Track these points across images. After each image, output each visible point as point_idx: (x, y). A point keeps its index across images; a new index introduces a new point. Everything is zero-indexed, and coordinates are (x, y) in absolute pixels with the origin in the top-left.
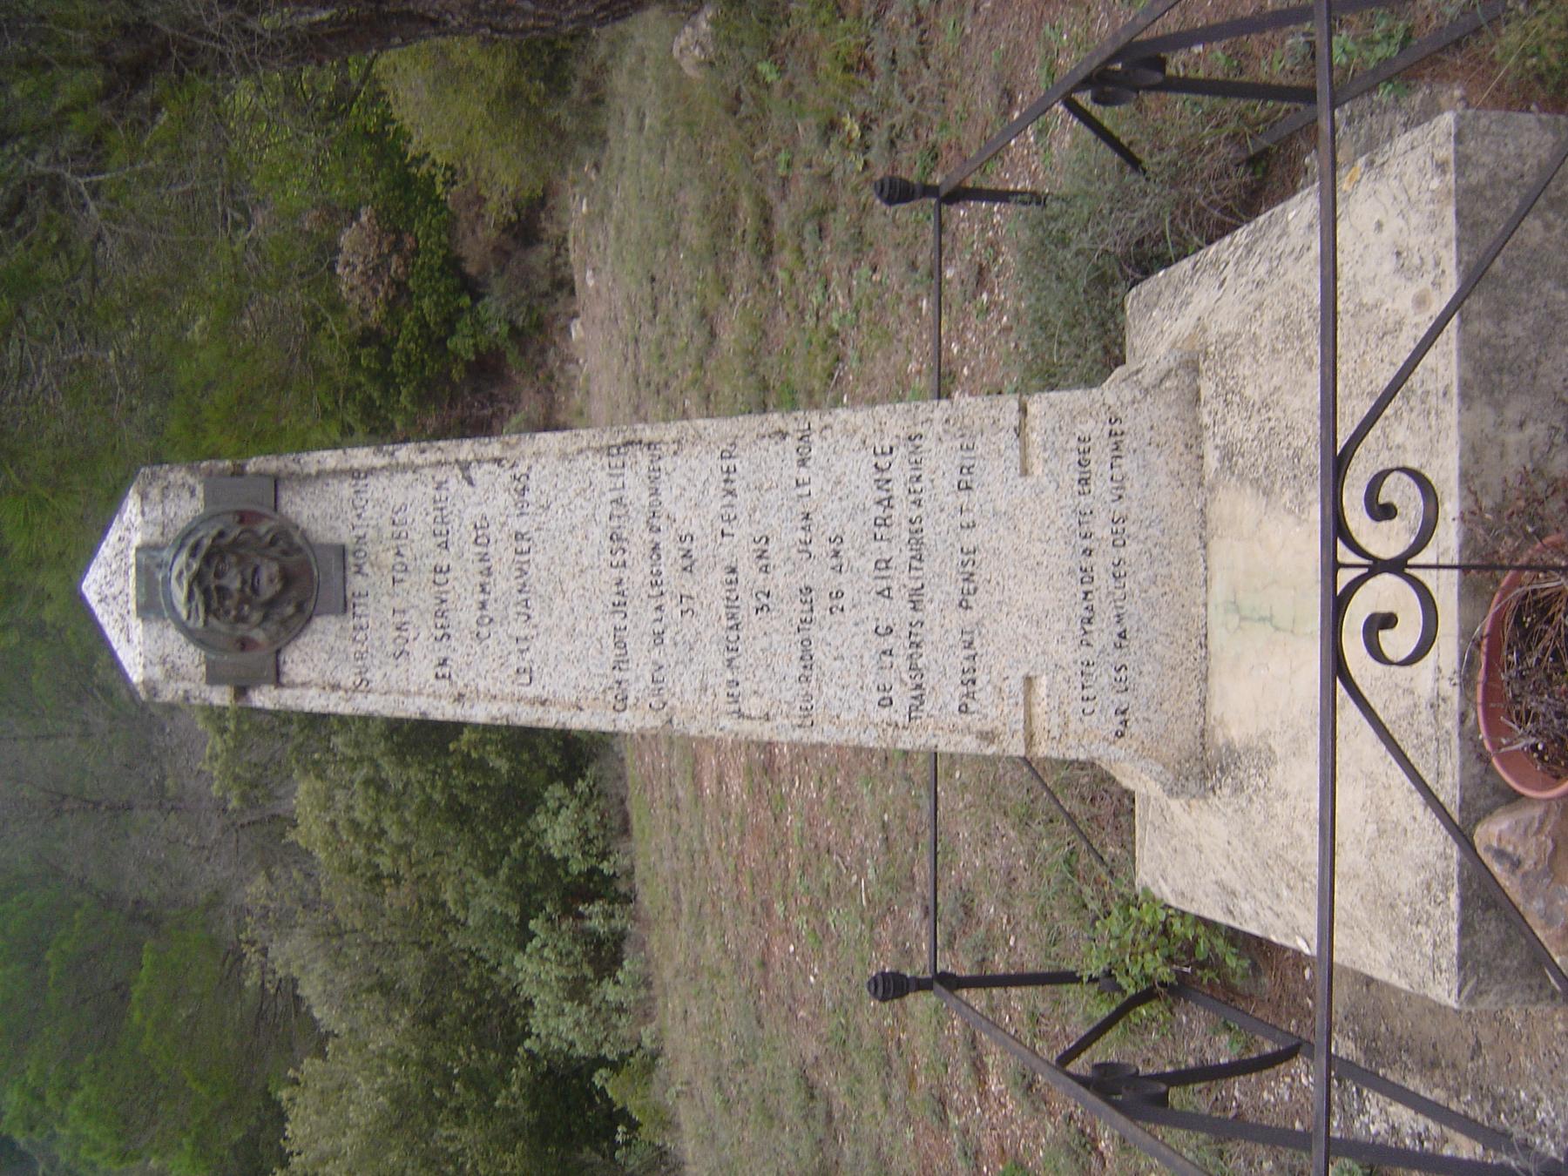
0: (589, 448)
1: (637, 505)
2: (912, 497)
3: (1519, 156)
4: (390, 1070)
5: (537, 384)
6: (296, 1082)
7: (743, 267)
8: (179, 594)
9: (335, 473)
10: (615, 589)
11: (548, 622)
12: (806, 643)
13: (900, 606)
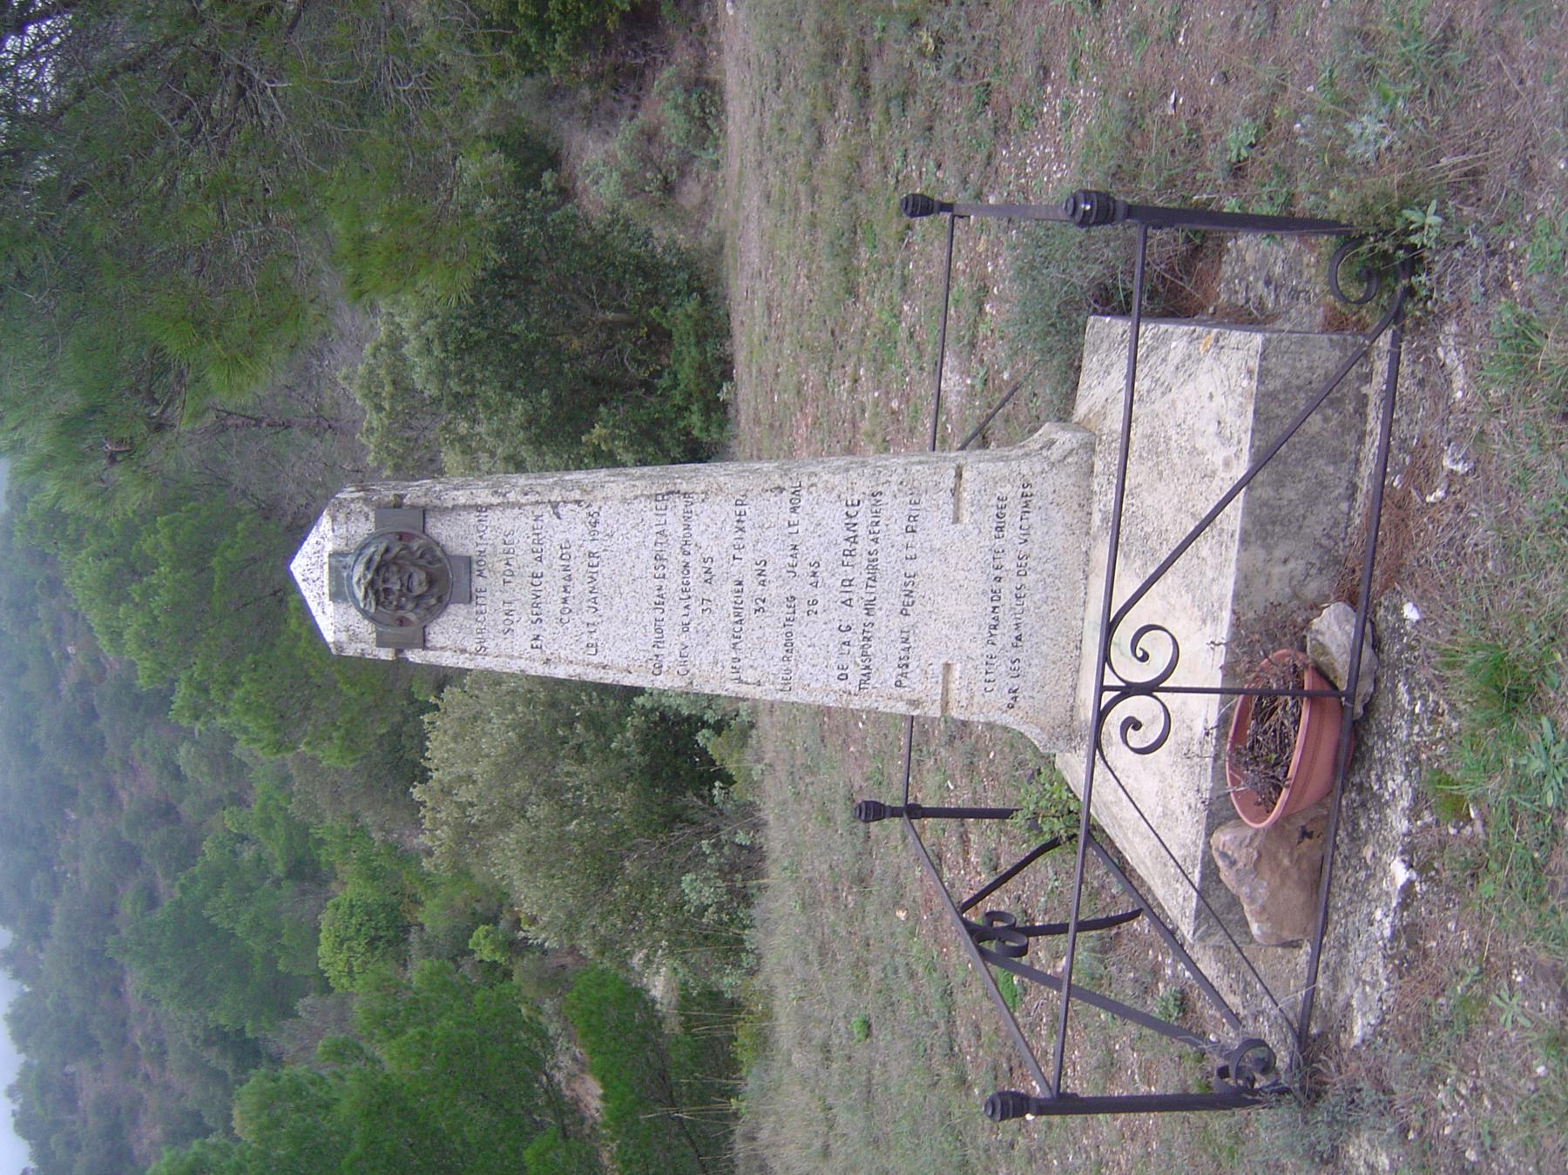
0: (642, 495)
1: (675, 536)
2: (872, 536)
3: (1310, 368)
4: (520, 709)
5: (690, 38)
6: (437, 708)
7: (846, 100)
8: (360, 594)
9: (465, 507)
10: (656, 593)
11: (609, 613)
12: (789, 634)
13: (857, 614)
